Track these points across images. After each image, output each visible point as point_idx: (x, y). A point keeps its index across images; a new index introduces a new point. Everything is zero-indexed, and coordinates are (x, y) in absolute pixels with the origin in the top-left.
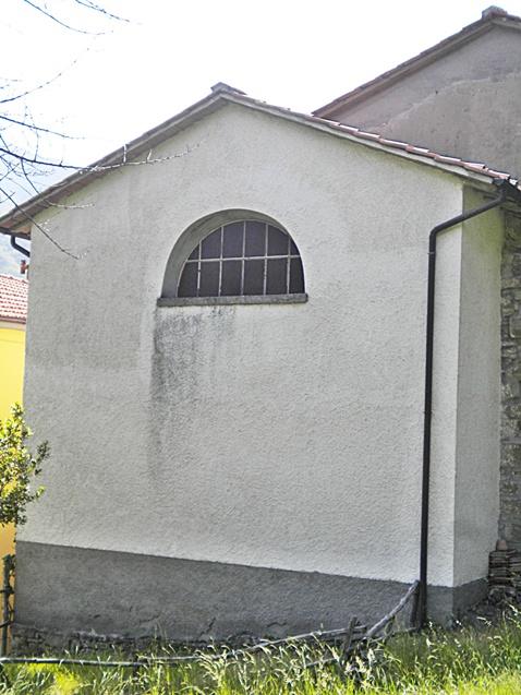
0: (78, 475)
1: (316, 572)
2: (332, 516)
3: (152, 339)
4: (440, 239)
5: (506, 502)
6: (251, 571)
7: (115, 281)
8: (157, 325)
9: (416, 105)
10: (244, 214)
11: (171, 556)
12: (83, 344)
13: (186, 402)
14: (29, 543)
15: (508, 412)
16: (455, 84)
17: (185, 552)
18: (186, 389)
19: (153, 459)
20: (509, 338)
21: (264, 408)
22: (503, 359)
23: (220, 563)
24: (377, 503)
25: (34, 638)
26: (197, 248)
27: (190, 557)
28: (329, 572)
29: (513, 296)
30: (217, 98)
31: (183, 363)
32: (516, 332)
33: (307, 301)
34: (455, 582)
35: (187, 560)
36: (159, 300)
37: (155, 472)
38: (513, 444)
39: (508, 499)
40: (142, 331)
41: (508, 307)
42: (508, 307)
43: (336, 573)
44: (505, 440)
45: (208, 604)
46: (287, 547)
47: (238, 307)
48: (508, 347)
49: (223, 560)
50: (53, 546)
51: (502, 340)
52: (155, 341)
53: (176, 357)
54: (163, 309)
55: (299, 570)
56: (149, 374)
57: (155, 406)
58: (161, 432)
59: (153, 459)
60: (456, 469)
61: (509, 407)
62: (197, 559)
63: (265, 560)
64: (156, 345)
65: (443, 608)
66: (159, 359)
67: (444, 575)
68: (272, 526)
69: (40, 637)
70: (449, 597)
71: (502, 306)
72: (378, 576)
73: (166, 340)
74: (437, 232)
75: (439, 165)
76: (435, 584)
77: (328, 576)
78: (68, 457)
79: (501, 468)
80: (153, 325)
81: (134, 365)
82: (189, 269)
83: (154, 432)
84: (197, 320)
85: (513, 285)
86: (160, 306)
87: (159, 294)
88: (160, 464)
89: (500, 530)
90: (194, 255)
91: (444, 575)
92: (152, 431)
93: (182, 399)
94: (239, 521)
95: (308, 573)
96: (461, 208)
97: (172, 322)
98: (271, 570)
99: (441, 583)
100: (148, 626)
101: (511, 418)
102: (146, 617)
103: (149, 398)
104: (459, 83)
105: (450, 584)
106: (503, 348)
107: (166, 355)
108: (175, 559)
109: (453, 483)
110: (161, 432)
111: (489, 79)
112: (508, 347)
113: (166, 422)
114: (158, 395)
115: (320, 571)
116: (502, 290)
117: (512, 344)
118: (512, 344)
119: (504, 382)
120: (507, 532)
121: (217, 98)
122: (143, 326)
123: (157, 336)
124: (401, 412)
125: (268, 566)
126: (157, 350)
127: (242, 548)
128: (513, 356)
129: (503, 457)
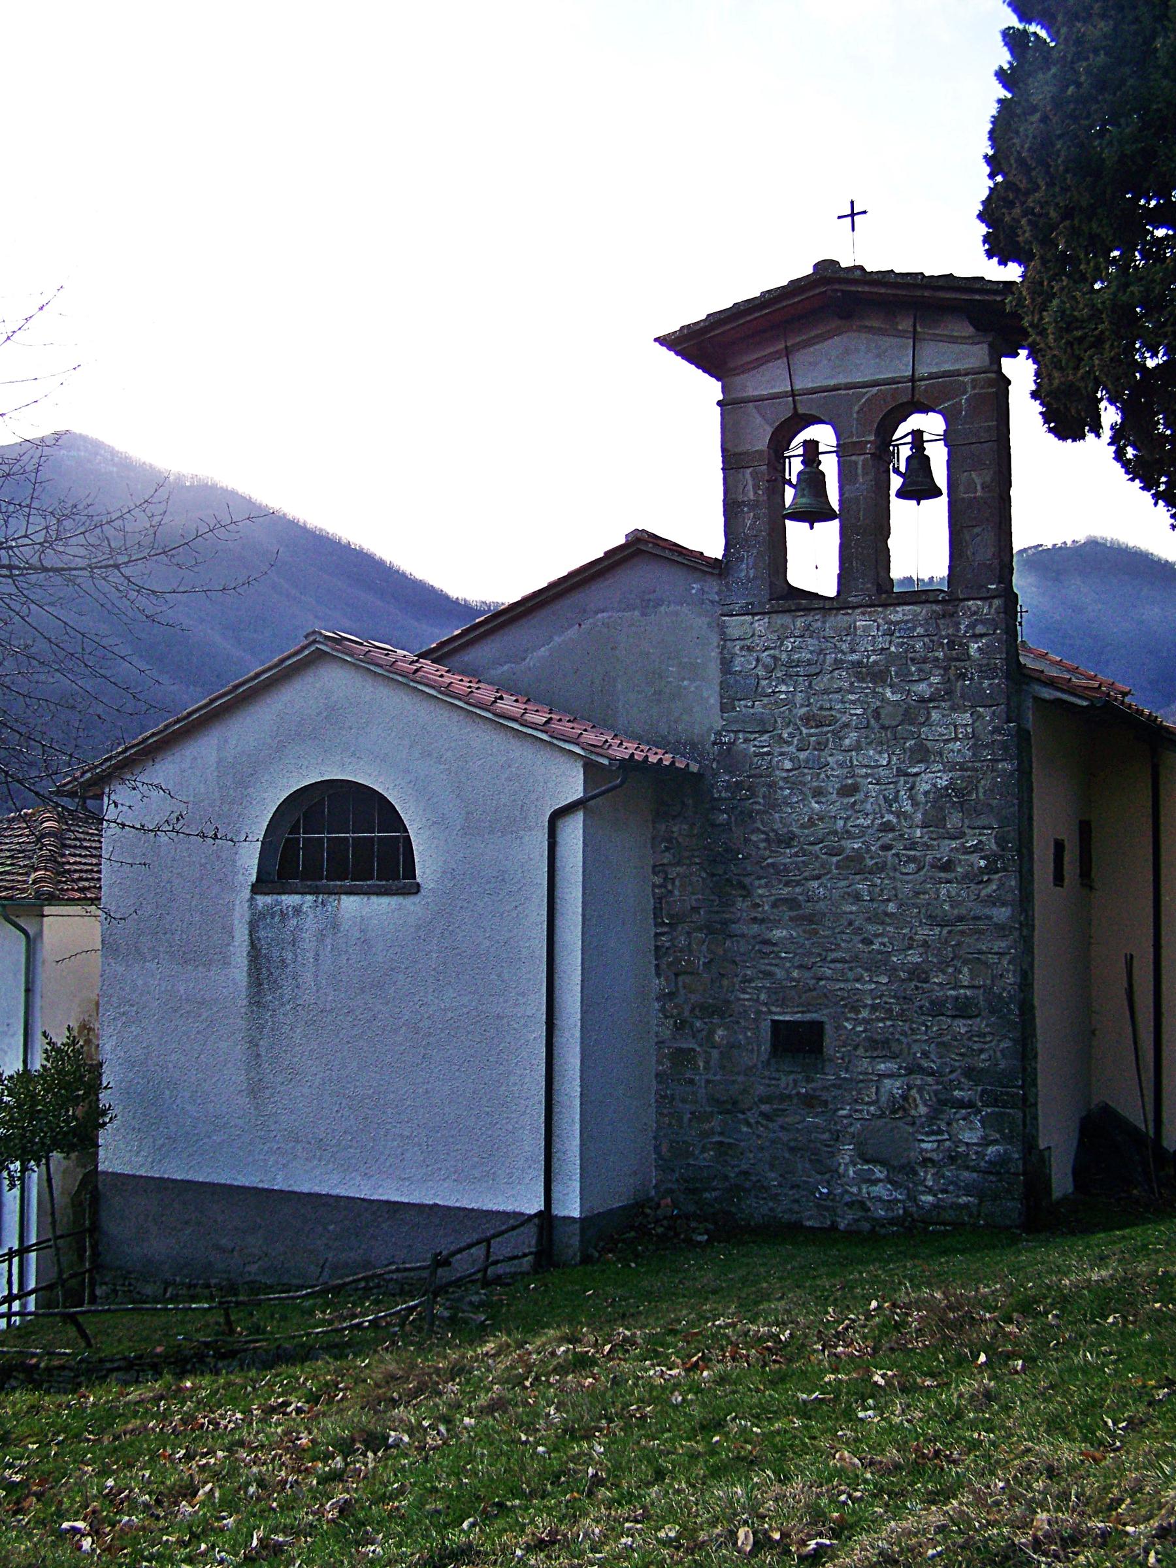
0: (167, 1092)
1: (436, 1205)
2: (451, 1140)
3: (247, 932)
4: (560, 824)
5: (661, 1114)
6: (365, 1204)
7: (203, 861)
8: (253, 914)
9: (556, 639)
10: (266, 890)
11: (276, 1188)
12: (168, 936)
13: (288, 1007)
14: (114, 1174)
15: (663, 1010)
16: (600, 616)
17: (291, 1182)
18: (287, 991)
19: (252, 1074)
20: (664, 924)
21: (375, 1017)
22: (657, 948)
23: (331, 1196)
24: (498, 1126)
25: (123, 1285)
26: (299, 820)
27: (296, 1189)
28: (450, 1203)
29: (666, 873)
30: (313, 648)
31: (283, 961)
32: (670, 917)
33: (418, 892)
34: (581, 1212)
35: (295, 1193)
36: (253, 885)
37: (255, 1090)
38: (669, 1048)
39: (665, 1111)
40: (236, 922)
41: (660, 886)
42: (660, 886)
43: (458, 1205)
44: (660, 1043)
45: (319, 1242)
46: (403, 1176)
47: (343, 897)
48: (662, 934)
49: (334, 1192)
50: (141, 1177)
51: (656, 925)
52: (251, 935)
53: (275, 954)
54: (258, 897)
55: (417, 1201)
56: (245, 974)
57: (252, 1012)
58: (261, 1043)
59: (252, 1074)
60: (581, 1086)
61: (664, 1004)
62: (306, 1191)
63: (381, 1190)
64: (251, 939)
65: (571, 1243)
66: (255, 953)
67: (570, 1206)
68: (387, 1152)
69: (130, 1284)
70: (577, 1226)
71: (654, 886)
72: (501, 1208)
73: (262, 934)
74: (558, 816)
75: (555, 742)
76: (562, 1214)
77: (448, 1208)
78: (155, 1071)
79: (657, 1075)
80: (247, 918)
81: (226, 963)
82: (291, 845)
83: (254, 1044)
84: (297, 911)
85: (665, 861)
86: (256, 893)
87: (254, 878)
88: (260, 1080)
89: (656, 1147)
90: (295, 829)
91: (570, 1206)
92: (250, 1042)
93: (283, 1005)
94: (351, 1147)
95: (427, 1205)
96: (581, 788)
97: (270, 912)
98: (388, 1202)
99: (565, 1213)
100: (253, 1268)
101: (666, 1017)
102: (250, 1259)
103: (245, 1002)
104: (605, 614)
105: (576, 1214)
106: (657, 935)
107: (264, 952)
108: (281, 1191)
109: (577, 1102)
110: (261, 1043)
111: (637, 613)
112: (662, 934)
113: (265, 1031)
114: (256, 999)
115: (440, 1203)
116: (654, 866)
117: (666, 929)
118: (666, 929)
119: (658, 975)
120: (664, 1149)
121: (313, 648)
122: (237, 915)
123: (253, 927)
124: (522, 1022)
125: (384, 1198)
126: (253, 944)
127: (353, 1179)
128: (668, 944)
129: (659, 1062)
